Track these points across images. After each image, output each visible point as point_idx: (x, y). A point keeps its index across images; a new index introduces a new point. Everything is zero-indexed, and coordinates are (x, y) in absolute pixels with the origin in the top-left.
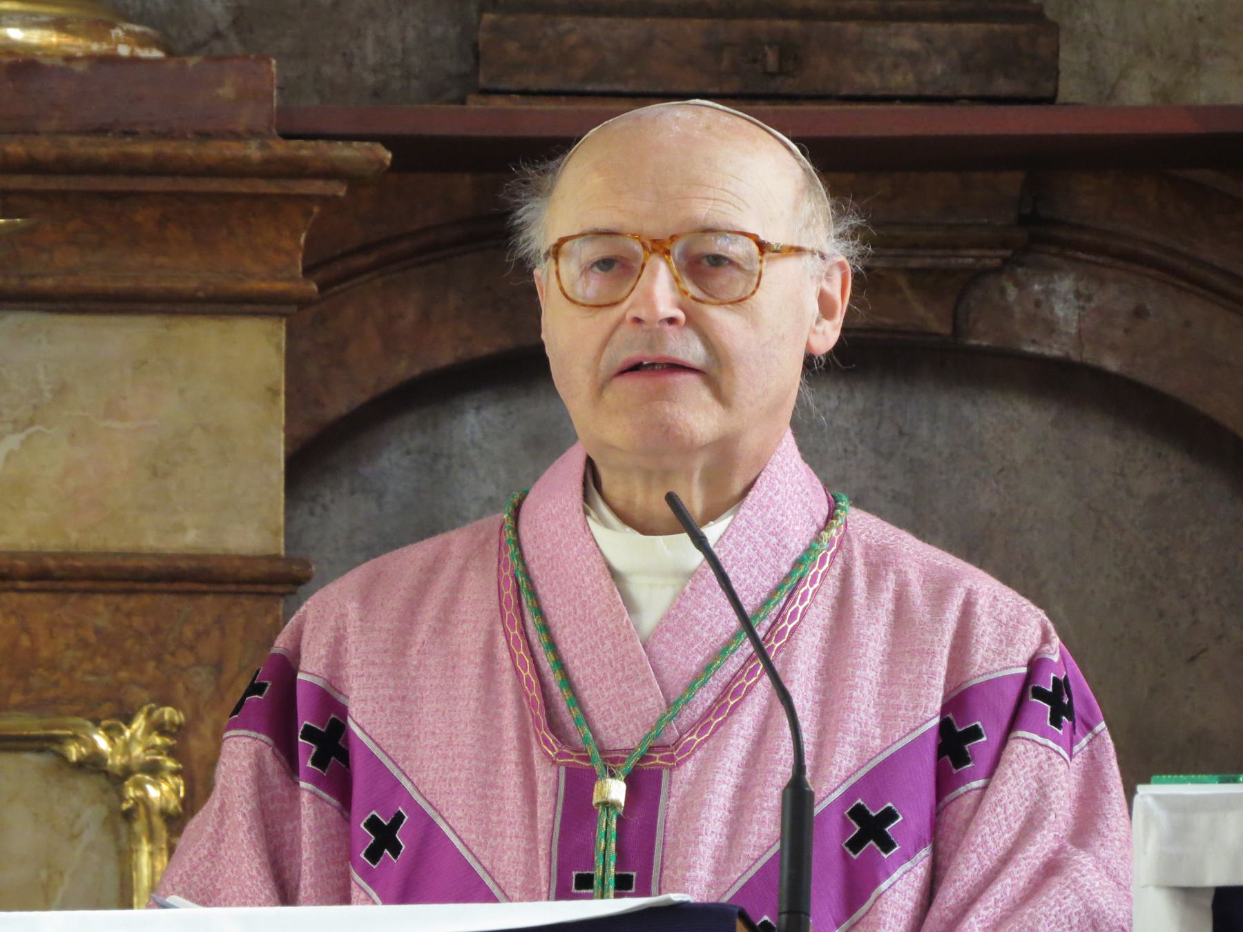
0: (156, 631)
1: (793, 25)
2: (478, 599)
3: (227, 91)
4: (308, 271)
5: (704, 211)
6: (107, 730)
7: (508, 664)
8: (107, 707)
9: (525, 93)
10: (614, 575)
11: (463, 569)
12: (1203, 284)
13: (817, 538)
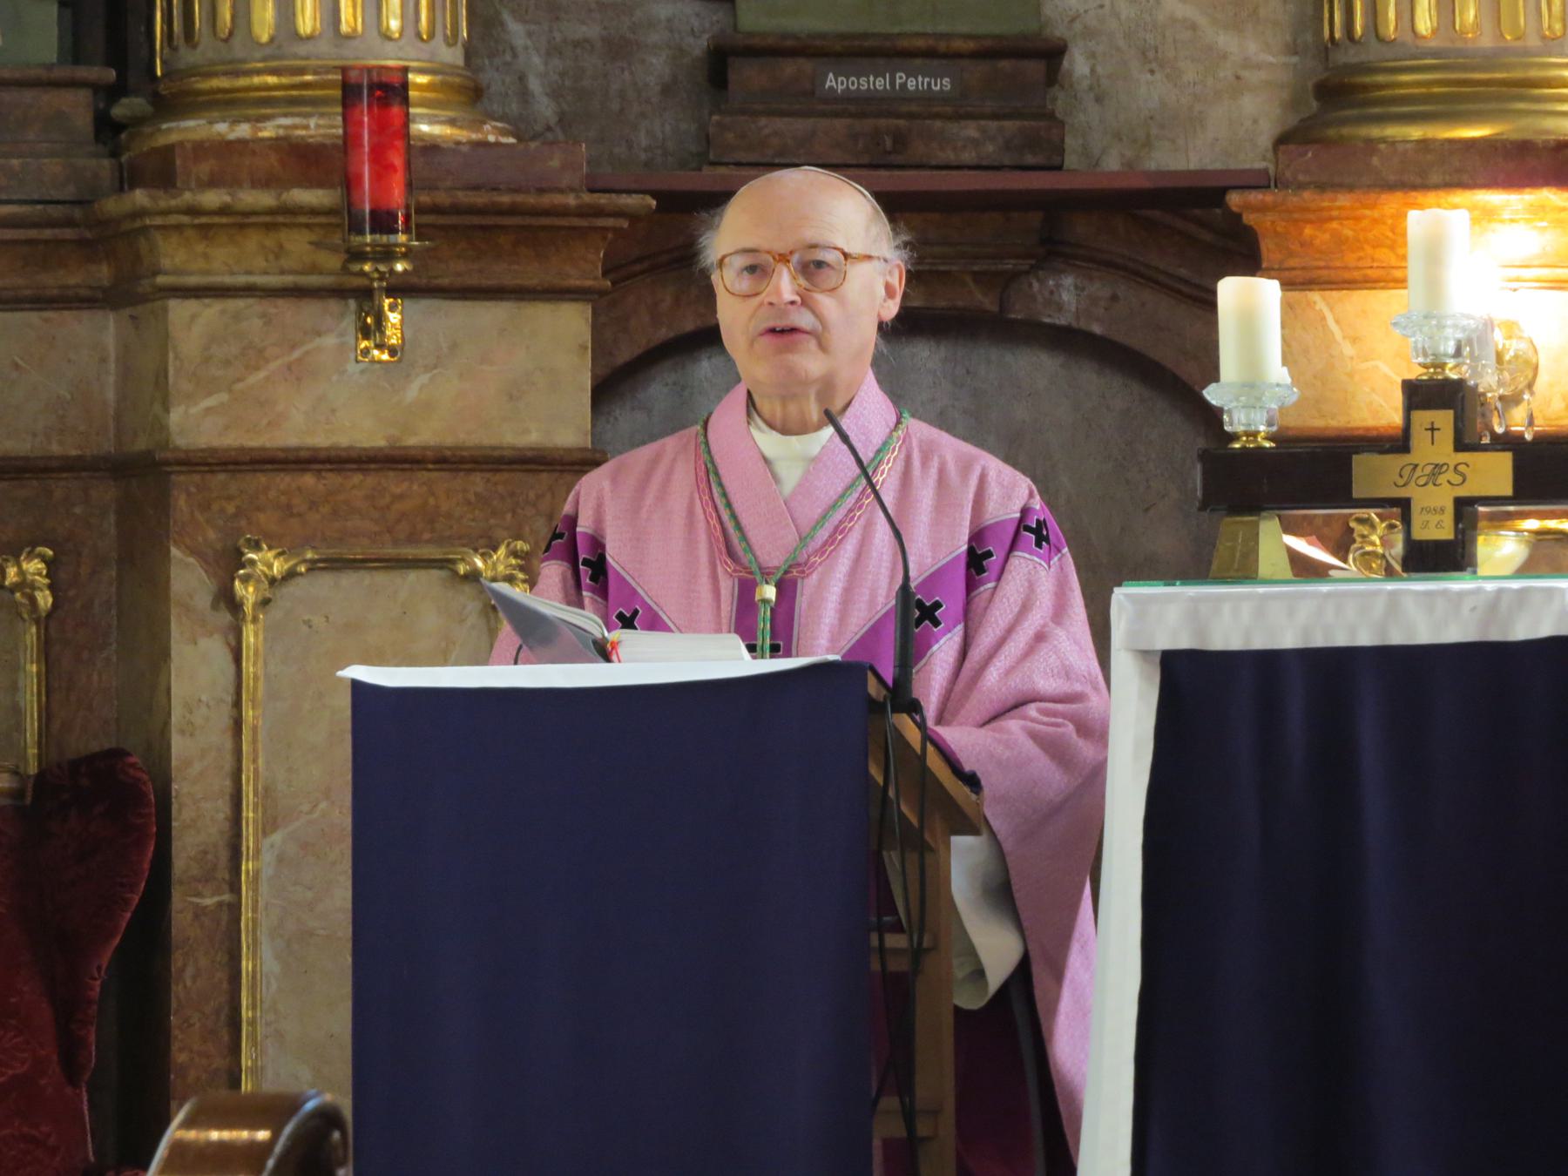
0: (512, 495)
1: (902, 122)
2: (683, 479)
3: (555, 163)
4: (605, 274)
5: (810, 235)
6: (482, 555)
7: (702, 517)
8: (482, 542)
9: (738, 164)
10: (766, 460)
11: (674, 460)
12: (1157, 282)
13: (890, 436)
